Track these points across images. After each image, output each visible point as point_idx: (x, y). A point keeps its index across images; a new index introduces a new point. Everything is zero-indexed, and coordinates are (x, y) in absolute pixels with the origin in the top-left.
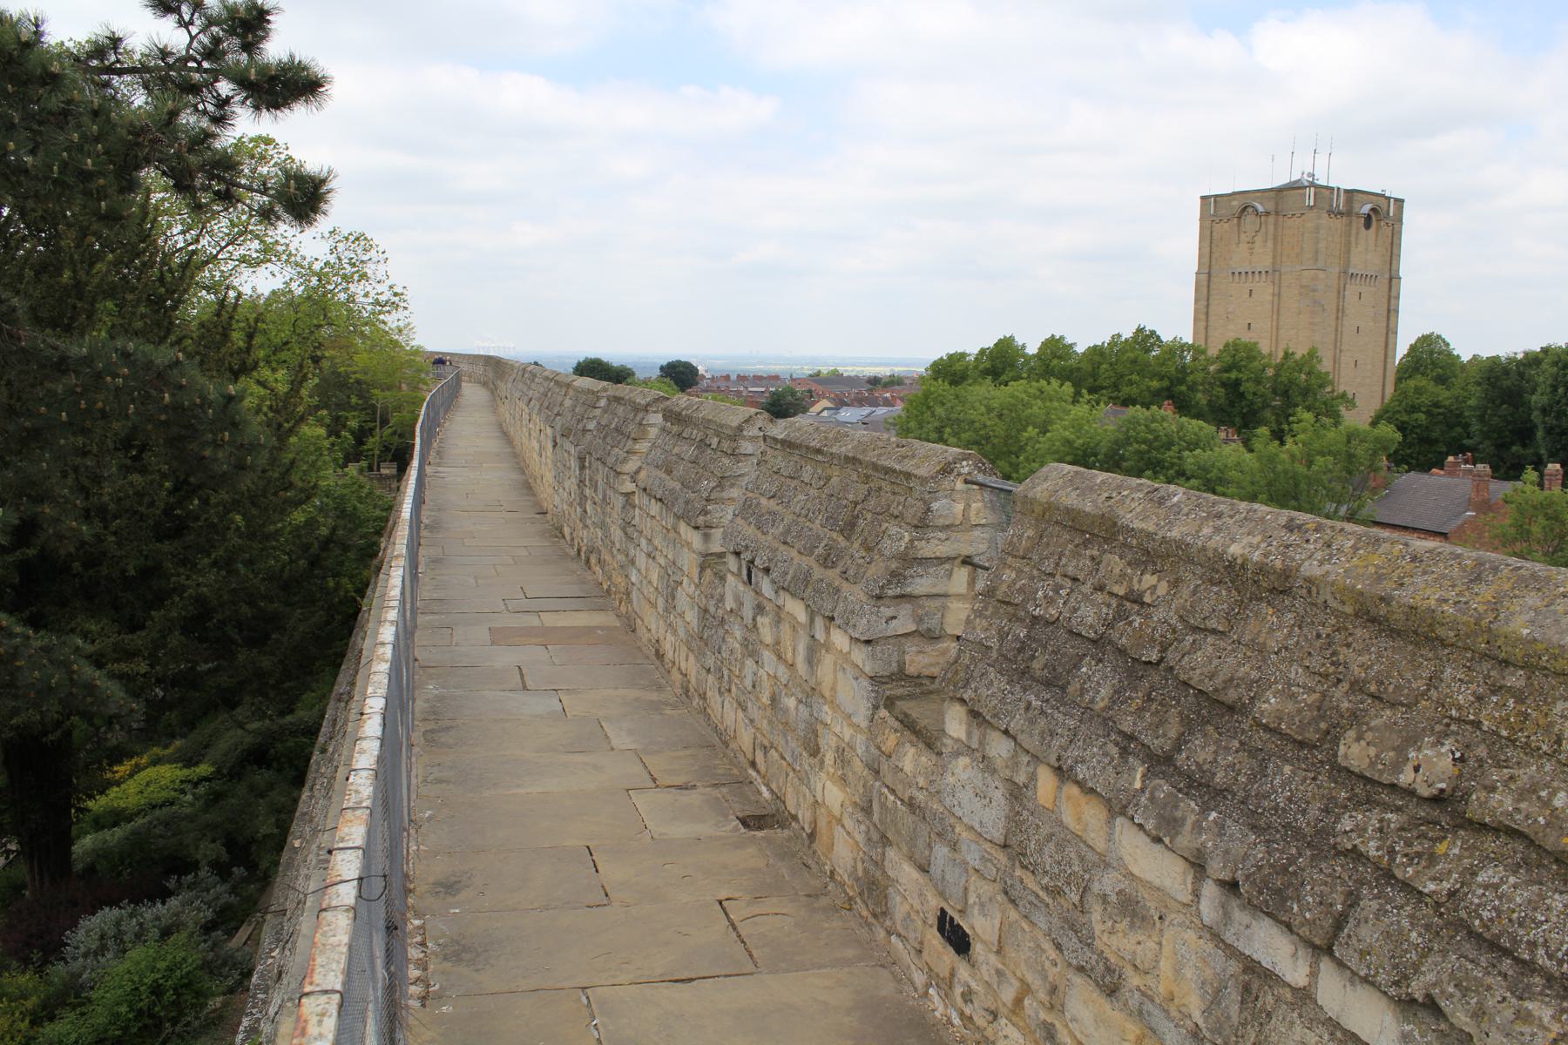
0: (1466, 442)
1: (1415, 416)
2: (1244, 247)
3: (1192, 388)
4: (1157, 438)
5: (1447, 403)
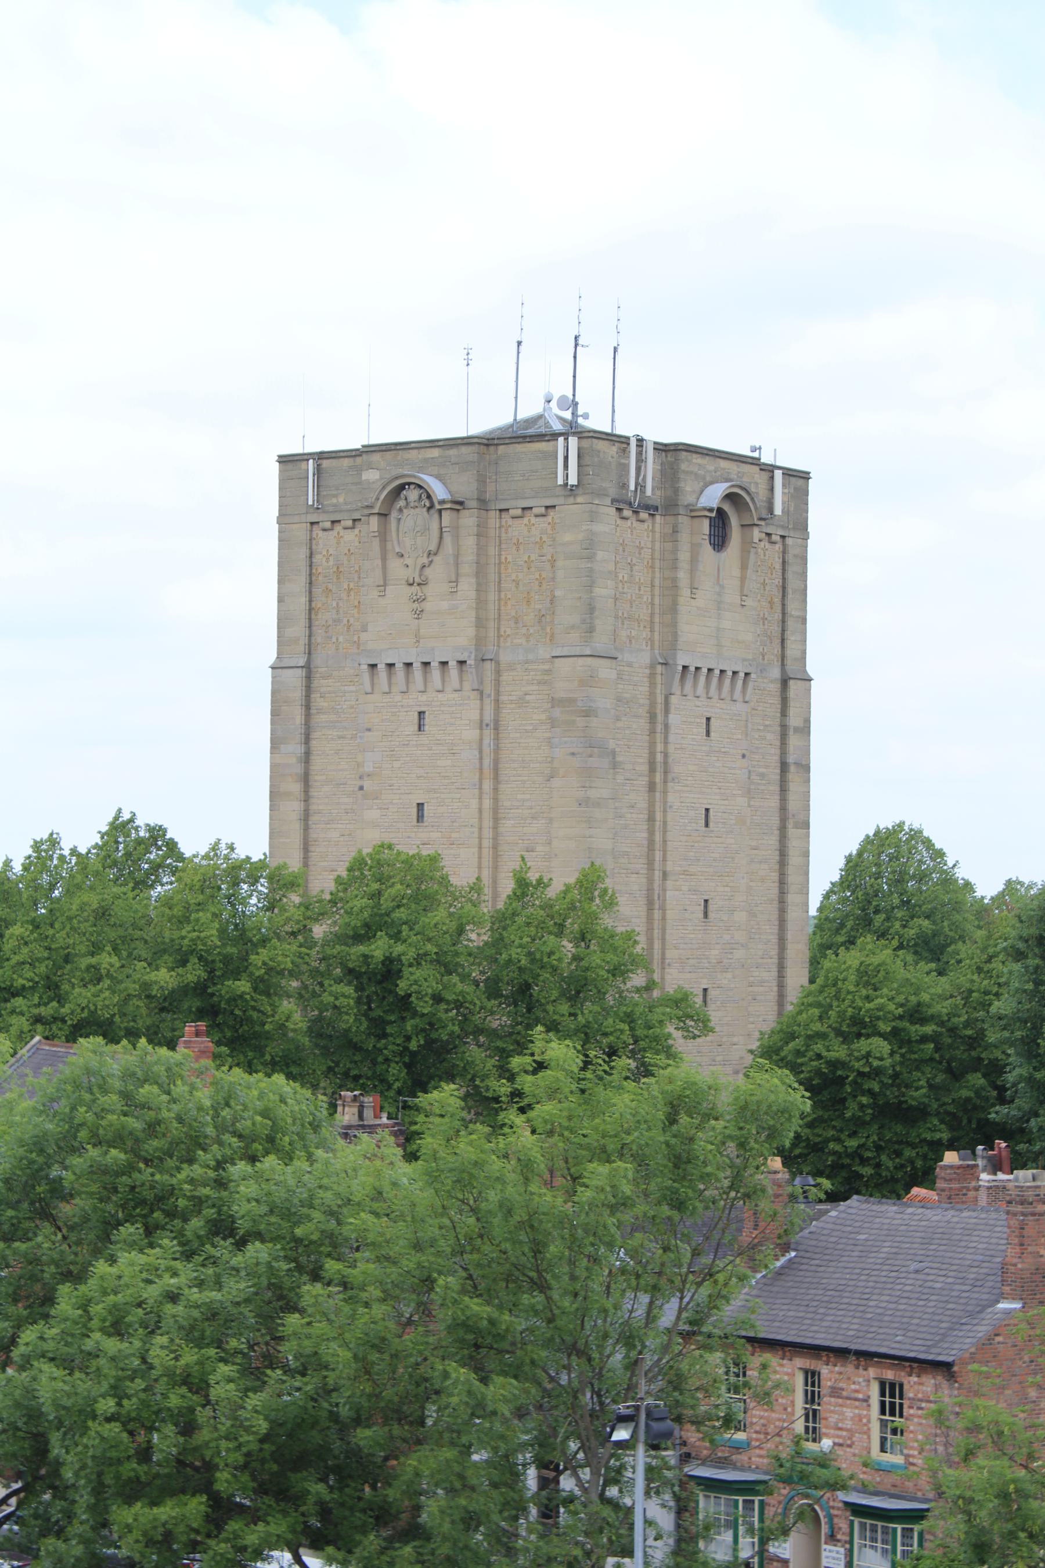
0: (998, 1113)
1: (863, 1045)
2: (399, 594)
4: (153, 1128)
5: (942, 1008)
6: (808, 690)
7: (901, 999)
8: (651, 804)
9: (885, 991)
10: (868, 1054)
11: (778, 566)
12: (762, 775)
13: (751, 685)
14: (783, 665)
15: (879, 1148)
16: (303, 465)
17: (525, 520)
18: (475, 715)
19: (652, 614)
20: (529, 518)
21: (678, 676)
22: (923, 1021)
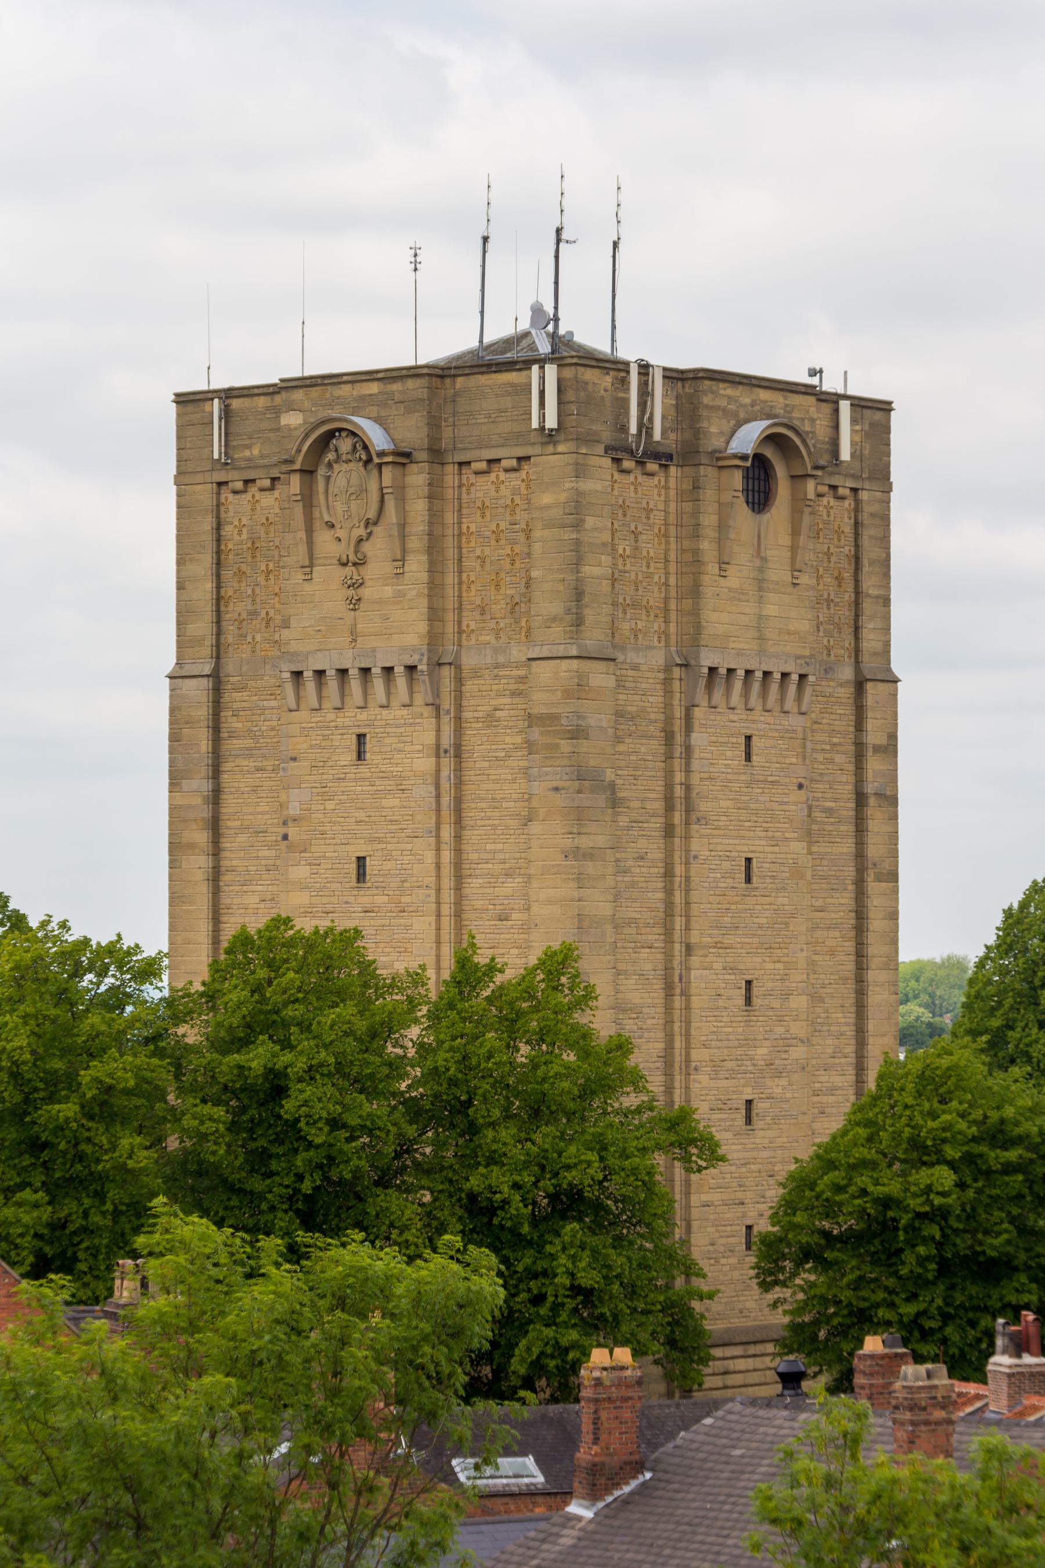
1: (923, 1177)
2: (329, 578)
3: (104, 1108)
6: (894, 695)
7: (977, 1114)
8: (669, 853)
9: (954, 1104)
10: (929, 1189)
11: (848, 529)
12: (829, 812)
13: (808, 691)
14: (857, 662)
15: (946, 1318)
16: (207, 404)
17: (493, 476)
18: (429, 738)
19: (666, 600)
20: (497, 474)
21: (703, 682)
22: (1009, 1143)
